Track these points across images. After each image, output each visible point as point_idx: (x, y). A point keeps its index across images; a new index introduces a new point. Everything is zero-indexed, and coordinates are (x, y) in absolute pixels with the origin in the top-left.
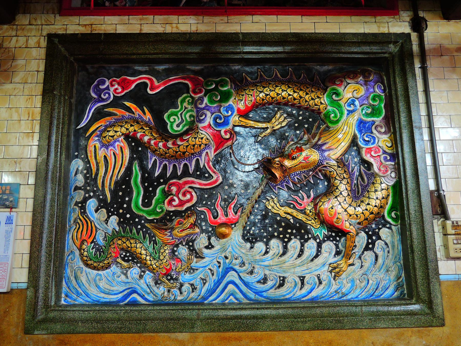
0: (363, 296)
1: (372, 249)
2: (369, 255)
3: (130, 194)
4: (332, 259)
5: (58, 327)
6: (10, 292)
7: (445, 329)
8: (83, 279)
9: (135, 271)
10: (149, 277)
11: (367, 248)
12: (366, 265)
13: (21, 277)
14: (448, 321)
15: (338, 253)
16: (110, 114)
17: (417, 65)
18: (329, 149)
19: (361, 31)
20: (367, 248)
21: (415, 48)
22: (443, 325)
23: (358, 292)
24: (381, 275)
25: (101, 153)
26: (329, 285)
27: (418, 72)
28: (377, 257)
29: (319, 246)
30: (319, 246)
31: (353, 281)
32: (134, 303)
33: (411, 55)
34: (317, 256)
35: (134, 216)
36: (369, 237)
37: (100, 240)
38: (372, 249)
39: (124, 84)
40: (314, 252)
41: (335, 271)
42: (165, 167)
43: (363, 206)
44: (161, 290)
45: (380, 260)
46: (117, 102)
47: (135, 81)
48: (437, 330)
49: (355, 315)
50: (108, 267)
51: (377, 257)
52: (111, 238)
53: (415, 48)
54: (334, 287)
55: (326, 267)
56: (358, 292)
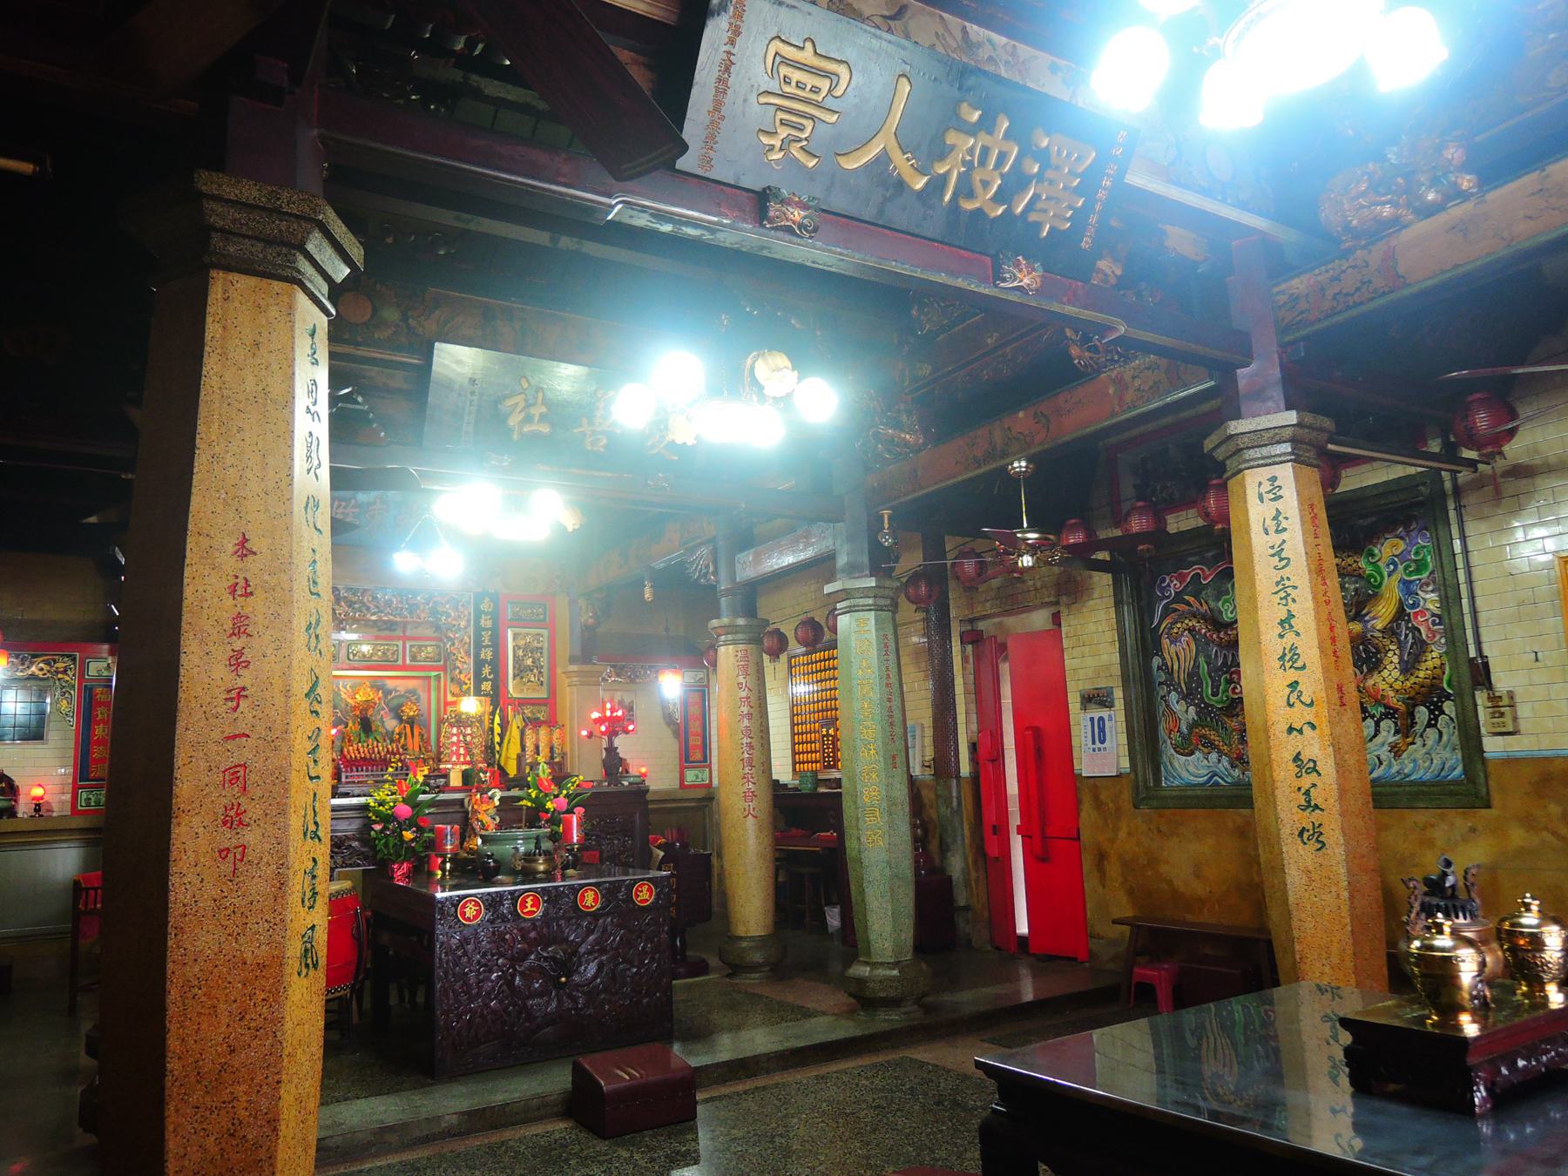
0: (1427, 777)
1: (1435, 726)
2: (1431, 734)
3: (1200, 685)
4: (1391, 739)
5: (1155, 803)
6: (1119, 776)
7: (1493, 812)
8: (1176, 764)
9: (1214, 756)
10: (1225, 761)
11: (1429, 725)
12: (1429, 743)
13: (1125, 764)
14: (1496, 799)
15: (1397, 732)
16: (1176, 610)
17: (1451, 505)
18: (1374, 618)
19: (1385, 479)
20: (1429, 725)
21: (1448, 485)
22: (1489, 807)
23: (1422, 772)
24: (1447, 754)
25: (1173, 649)
26: (1390, 766)
27: (1452, 514)
28: (1441, 734)
29: (1377, 724)
30: (1377, 724)
31: (1414, 761)
32: (1217, 784)
33: (1443, 495)
34: (1375, 736)
35: (1207, 705)
36: (1431, 712)
37: (1184, 729)
38: (1435, 726)
39: (1181, 578)
40: (1372, 731)
41: (1396, 751)
42: (1225, 657)
43: (1413, 679)
44: (1236, 773)
45: (1445, 738)
46: (1178, 598)
47: (1190, 573)
48: (1484, 812)
49: (1396, 794)
50: (1192, 753)
51: (1441, 734)
52: (1193, 726)
53: (1448, 485)
54: (1395, 769)
55: (1387, 748)
56: (1422, 772)
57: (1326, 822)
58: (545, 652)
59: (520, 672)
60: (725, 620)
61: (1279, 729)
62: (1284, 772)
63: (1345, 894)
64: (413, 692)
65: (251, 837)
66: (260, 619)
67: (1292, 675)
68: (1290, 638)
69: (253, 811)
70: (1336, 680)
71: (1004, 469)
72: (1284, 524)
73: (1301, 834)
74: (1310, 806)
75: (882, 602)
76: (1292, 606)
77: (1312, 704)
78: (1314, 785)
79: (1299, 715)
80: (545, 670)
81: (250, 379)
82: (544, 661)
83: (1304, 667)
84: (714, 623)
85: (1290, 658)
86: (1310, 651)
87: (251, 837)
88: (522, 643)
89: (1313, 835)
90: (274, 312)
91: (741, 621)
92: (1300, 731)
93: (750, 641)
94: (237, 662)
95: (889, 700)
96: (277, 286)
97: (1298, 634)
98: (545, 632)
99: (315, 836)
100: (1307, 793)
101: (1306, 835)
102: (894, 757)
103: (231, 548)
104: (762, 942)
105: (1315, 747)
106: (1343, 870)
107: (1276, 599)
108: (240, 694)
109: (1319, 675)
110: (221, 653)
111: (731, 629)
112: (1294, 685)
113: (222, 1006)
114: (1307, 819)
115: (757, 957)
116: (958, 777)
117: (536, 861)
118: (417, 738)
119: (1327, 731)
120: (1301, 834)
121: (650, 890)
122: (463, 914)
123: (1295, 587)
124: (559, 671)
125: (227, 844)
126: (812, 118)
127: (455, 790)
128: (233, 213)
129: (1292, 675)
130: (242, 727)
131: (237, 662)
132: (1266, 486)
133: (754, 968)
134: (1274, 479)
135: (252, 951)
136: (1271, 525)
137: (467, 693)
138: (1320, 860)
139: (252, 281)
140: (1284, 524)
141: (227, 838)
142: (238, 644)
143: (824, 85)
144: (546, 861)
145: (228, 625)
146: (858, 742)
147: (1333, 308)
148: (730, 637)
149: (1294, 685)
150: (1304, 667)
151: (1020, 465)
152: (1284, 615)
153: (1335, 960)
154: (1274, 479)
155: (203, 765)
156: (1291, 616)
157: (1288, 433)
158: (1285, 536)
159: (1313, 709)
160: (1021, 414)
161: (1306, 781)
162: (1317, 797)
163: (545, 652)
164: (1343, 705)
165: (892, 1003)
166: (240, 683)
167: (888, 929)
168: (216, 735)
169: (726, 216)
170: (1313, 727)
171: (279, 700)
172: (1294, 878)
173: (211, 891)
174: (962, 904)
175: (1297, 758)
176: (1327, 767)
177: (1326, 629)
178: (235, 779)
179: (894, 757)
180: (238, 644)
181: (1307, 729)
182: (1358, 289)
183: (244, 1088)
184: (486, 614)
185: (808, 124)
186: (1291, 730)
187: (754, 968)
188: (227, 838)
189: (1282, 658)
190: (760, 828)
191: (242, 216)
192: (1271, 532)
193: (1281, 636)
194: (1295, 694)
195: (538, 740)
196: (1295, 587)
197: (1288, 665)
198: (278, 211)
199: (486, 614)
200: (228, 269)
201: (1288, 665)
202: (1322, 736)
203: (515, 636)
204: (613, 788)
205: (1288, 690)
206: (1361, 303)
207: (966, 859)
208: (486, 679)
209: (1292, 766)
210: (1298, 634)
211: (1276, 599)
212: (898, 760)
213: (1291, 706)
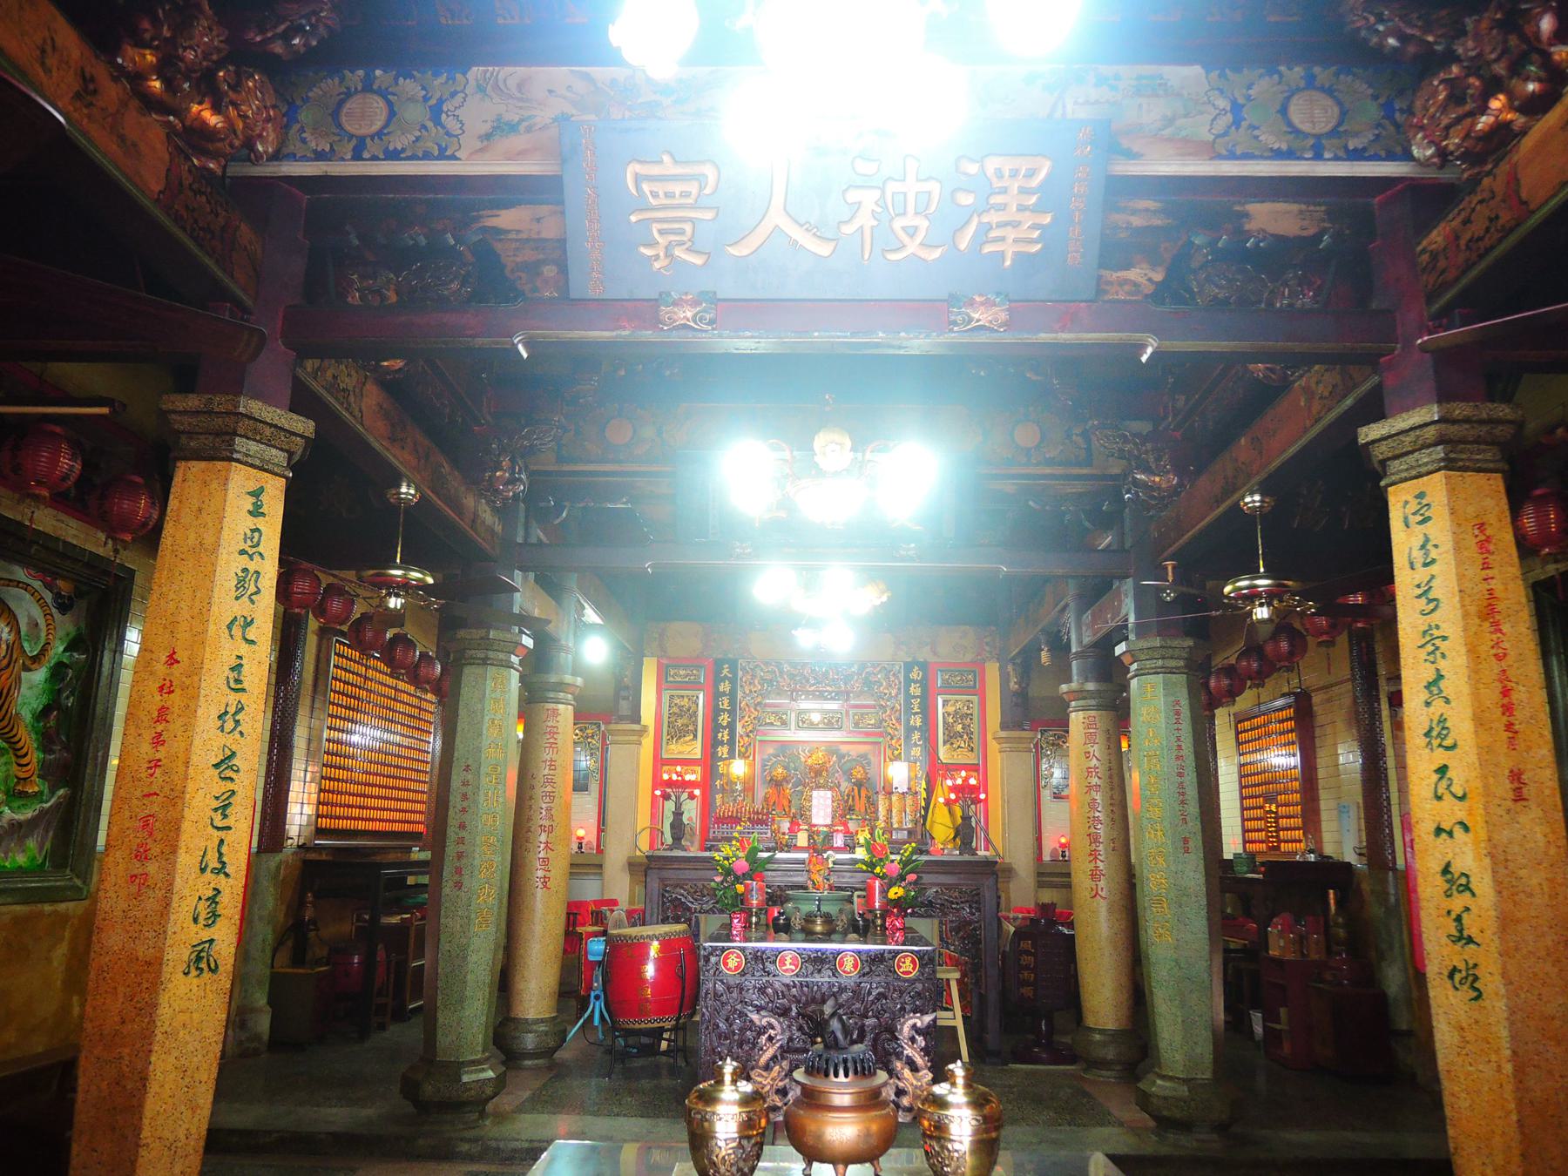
57: (1481, 961)
58: (975, 717)
59: (951, 737)
60: (1074, 685)
61: (1423, 830)
62: (1429, 889)
63: (1508, 1068)
64: (864, 756)
65: (152, 868)
66: (176, 709)
67: (1440, 757)
68: (1439, 706)
69: (155, 850)
70: (1506, 764)
71: (1236, 508)
72: (1434, 554)
73: (1451, 976)
74: (1463, 938)
75: (1173, 663)
76: (1442, 664)
77: (1462, 798)
78: (1467, 909)
79: (1451, 811)
80: (975, 737)
81: (192, 536)
82: (975, 727)
83: (1454, 746)
84: (1064, 687)
85: (1438, 733)
86: (1462, 727)
87: (152, 868)
88: (951, 709)
89: (1469, 979)
90: (214, 485)
91: (1091, 686)
92: (1450, 834)
93: (1099, 707)
94: (158, 741)
95: (1180, 775)
96: (219, 464)
97: (1447, 701)
98: (975, 699)
99: (221, 870)
100: (1459, 919)
101: (1457, 977)
102: (1186, 840)
103: (164, 658)
104: (1115, 1036)
105: (1467, 856)
106: (1505, 1033)
107: (1423, 654)
108: (156, 764)
109: (1473, 758)
110: (148, 735)
111: (1080, 694)
112: (1442, 770)
113: (121, 989)
114: (1457, 956)
115: (1110, 1053)
116: (1394, 869)
117: (814, 922)
118: (863, 800)
119: (1483, 835)
120: (1451, 976)
121: (913, 962)
122: (726, 964)
123: (1444, 638)
124: (989, 737)
125: (135, 872)
126: (690, 220)
127: (802, 849)
128: (186, 419)
129: (1440, 757)
130: (155, 788)
131: (158, 741)
132: (1413, 506)
133: (1101, 1064)
134: (1421, 496)
135: (142, 951)
136: (1418, 555)
137: (898, 758)
138: (1476, 1015)
139: (203, 464)
140: (1434, 554)
141: (136, 867)
142: (160, 728)
143: (693, 188)
144: (824, 923)
145: (155, 714)
146: (1145, 822)
147: (1467, 260)
148: (1081, 703)
149: (1442, 770)
150: (1454, 746)
151: (1253, 500)
152: (1431, 676)
153: (1500, 1160)
154: (1421, 496)
155: (127, 814)
156: (1440, 677)
157: (1430, 433)
158: (1434, 569)
159: (1465, 804)
160: (1243, 441)
161: (1458, 902)
162: (1471, 926)
163: (975, 717)
164: (1519, 798)
165: (1184, 1126)
166: (158, 756)
167: (1178, 1039)
168: (138, 793)
169: (624, 328)
170: (1466, 829)
171: (182, 769)
172: (1444, 1036)
173: (123, 905)
174: (1404, 1027)
175: (1446, 870)
176: (1483, 884)
177: (1492, 696)
178: (145, 825)
179: (1186, 840)
180: (160, 728)
181: (1458, 832)
182: (1487, 230)
183: (127, 1050)
184: (916, 682)
185: (688, 227)
186: (1439, 831)
187: (1101, 1064)
188: (136, 867)
189: (1427, 734)
190: (1110, 910)
191: (194, 421)
192: (1418, 565)
193: (1428, 704)
194: (1444, 783)
195: (890, 805)
196: (1444, 638)
197: (1435, 743)
198: (210, 412)
199: (916, 682)
200: (187, 459)
201: (1435, 743)
202: (1476, 842)
203: (945, 703)
204: (967, 857)
205: (1435, 777)
206: (1493, 247)
207: (1405, 970)
208: (916, 745)
209: (1439, 880)
210: (1447, 701)
211: (1423, 654)
212: (1191, 844)
213: (1439, 798)
